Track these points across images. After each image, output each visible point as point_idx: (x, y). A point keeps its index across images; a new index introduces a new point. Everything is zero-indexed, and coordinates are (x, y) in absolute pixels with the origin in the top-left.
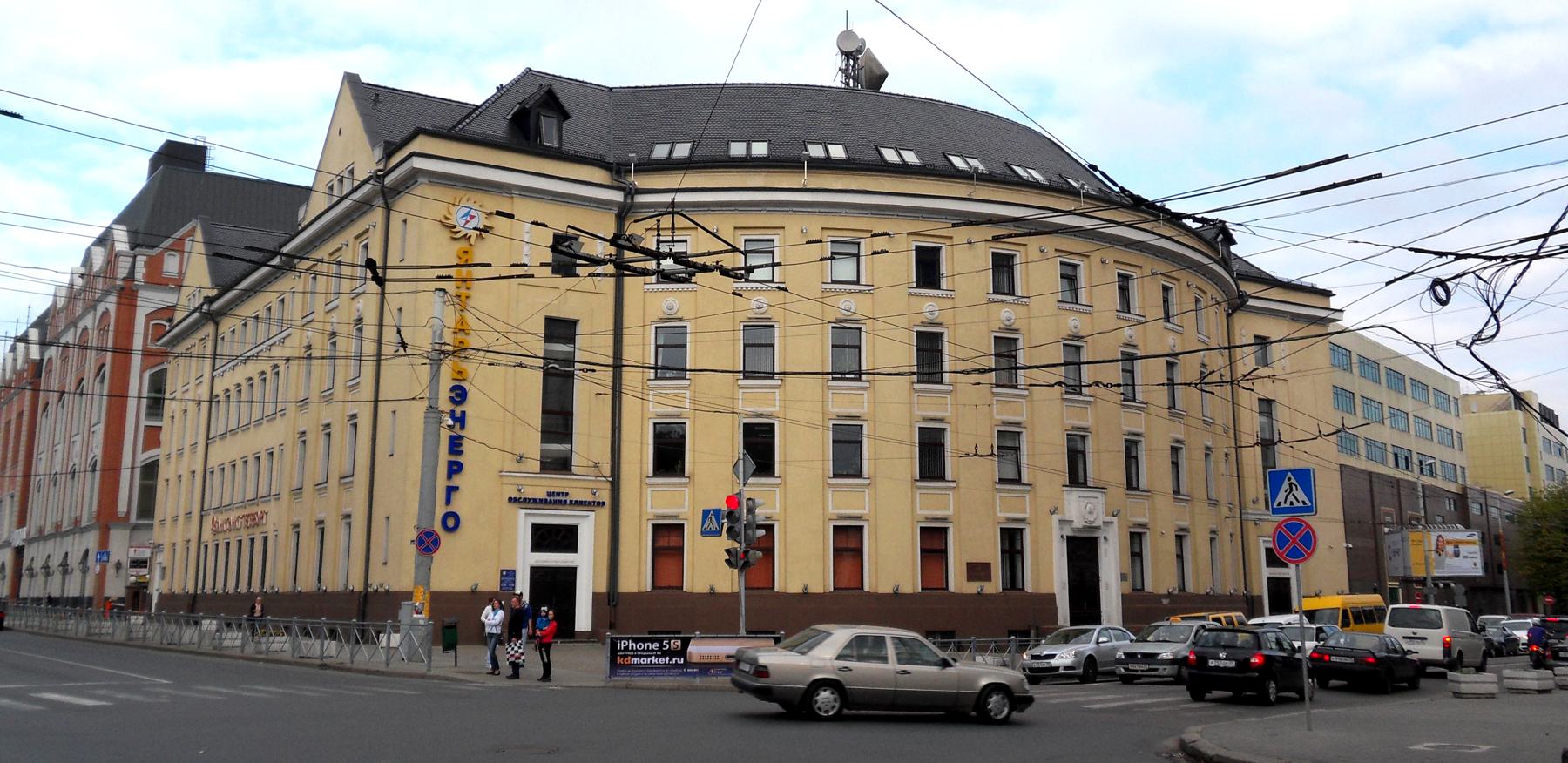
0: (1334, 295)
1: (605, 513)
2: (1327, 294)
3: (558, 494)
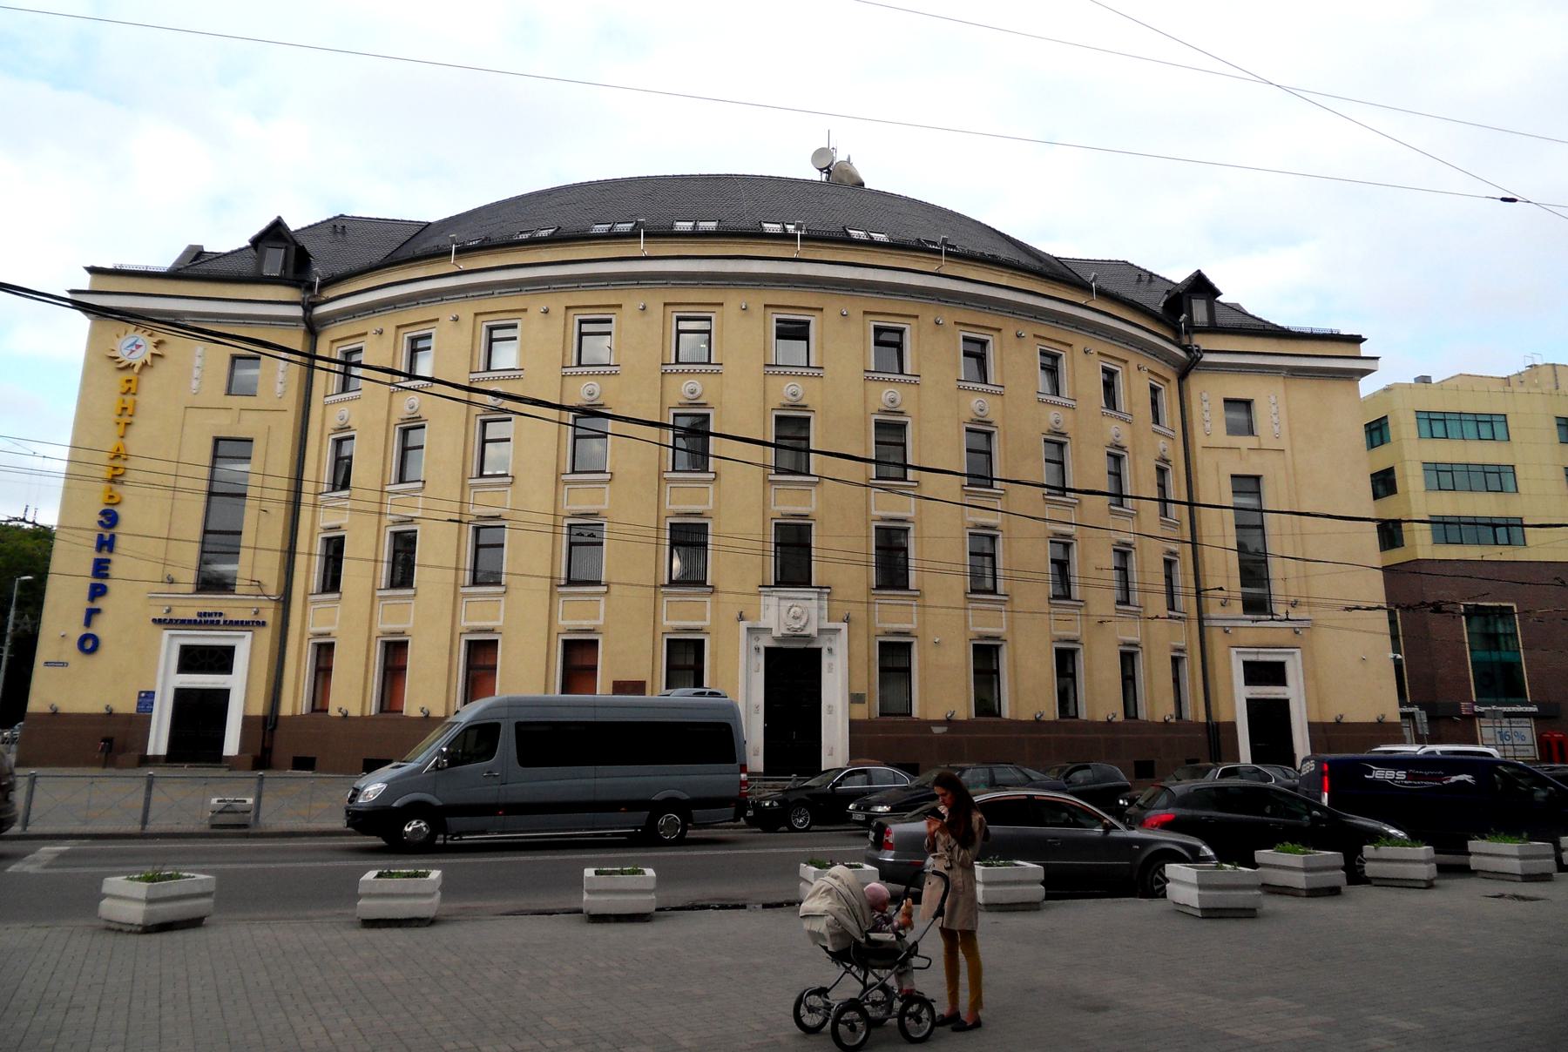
0: (1365, 340)
1: (266, 636)
2: (1357, 340)
3: (210, 615)
